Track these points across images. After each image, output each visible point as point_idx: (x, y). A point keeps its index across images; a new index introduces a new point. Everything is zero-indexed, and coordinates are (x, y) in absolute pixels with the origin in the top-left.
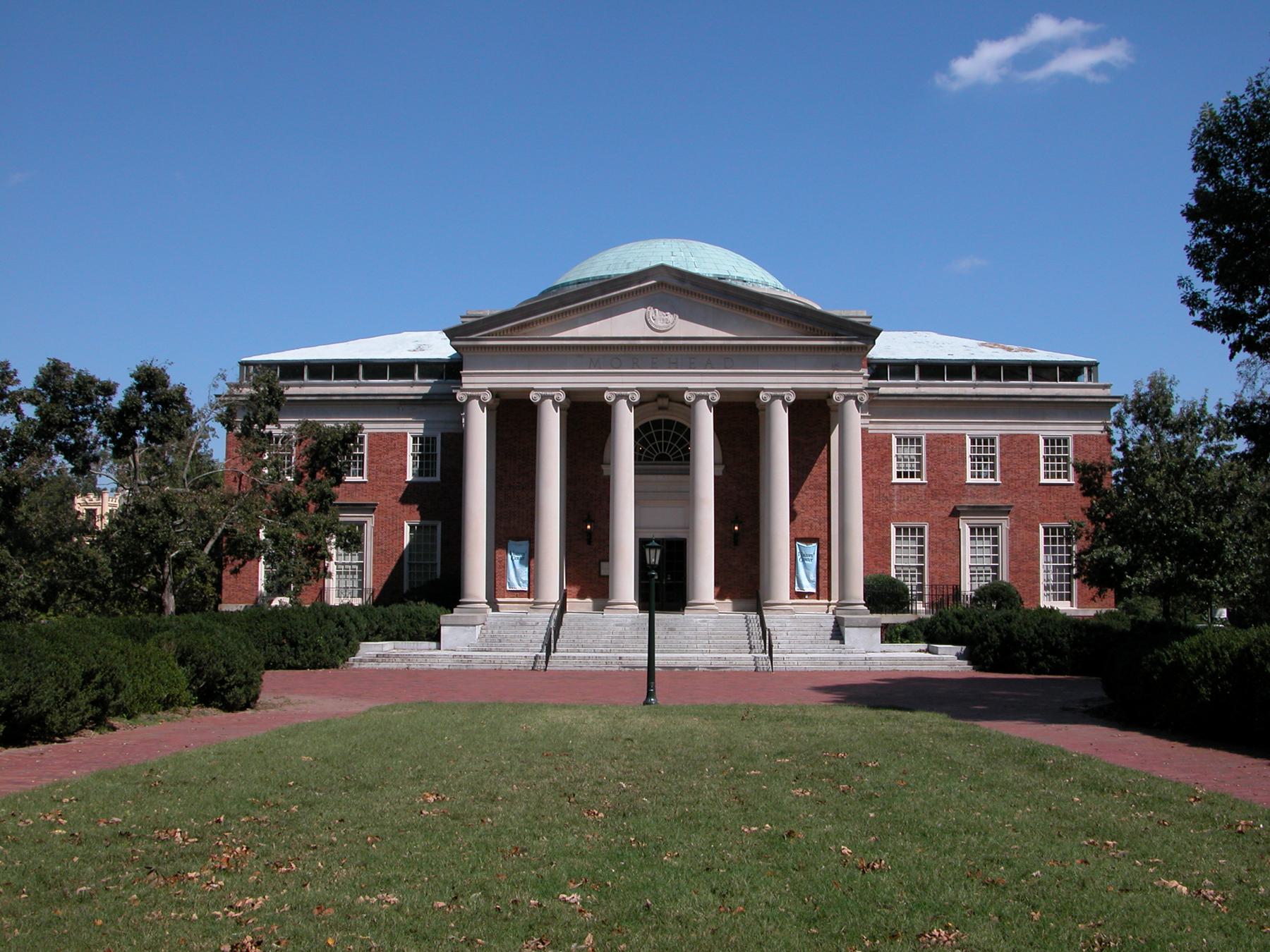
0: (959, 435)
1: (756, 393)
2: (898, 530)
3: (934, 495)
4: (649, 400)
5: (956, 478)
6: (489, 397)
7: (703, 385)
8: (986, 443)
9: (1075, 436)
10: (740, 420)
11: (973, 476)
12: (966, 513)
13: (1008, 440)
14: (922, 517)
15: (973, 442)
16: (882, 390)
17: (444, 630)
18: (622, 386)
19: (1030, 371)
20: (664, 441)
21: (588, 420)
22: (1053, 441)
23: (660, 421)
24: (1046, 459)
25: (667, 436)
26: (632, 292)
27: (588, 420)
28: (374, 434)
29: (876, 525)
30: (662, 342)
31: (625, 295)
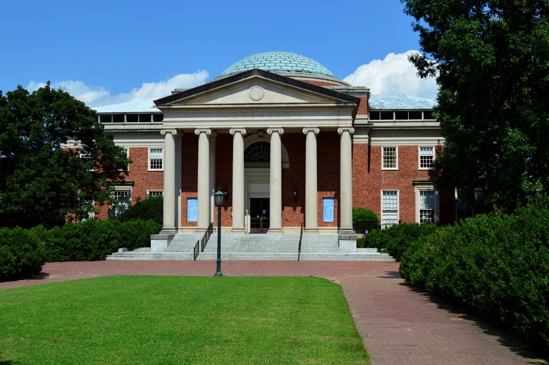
0: (415, 146)
1: (302, 128)
3: (402, 176)
4: (249, 134)
5: (413, 167)
6: (175, 132)
7: (275, 125)
8: (391, 150)
9: (130, 148)
10: (293, 140)
12: (418, 184)
13: (403, 149)
14: (397, 186)
15: (385, 149)
18: (238, 125)
19: (152, 116)
20: (258, 152)
21: (222, 141)
22: (388, 149)
23: (260, 142)
24: (385, 158)
25: (259, 149)
26: (242, 82)
27: (222, 141)
28: (132, 148)
29: (373, 190)
30: (256, 106)
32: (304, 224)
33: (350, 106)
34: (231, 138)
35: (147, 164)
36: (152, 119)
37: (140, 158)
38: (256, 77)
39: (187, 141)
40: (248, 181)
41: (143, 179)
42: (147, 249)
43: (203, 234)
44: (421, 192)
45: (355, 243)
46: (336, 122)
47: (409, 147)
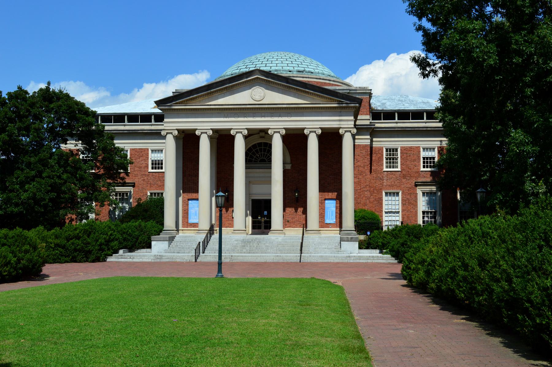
0: (417, 147)
2: (386, 193)
3: (404, 177)
4: (251, 134)
5: (416, 168)
7: (277, 126)
8: (393, 151)
9: (130, 149)
10: (295, 141)
11: (152, 168)
13: (405, 150)
14: (399, 187)
15: (387, 150)
16: (377, 125)
17: (153, 243)
18: (239, 126)
19: (153, 117)
20: (259, 153)
21: (223, 142)
22: (390, 150)
23: (261, 143)
24: (387, 159)
25: (261, 150)
26: (243, 82)
27: (223, 142)
29: (375, 191)
30: (257, 106)
31: (238, 84)
32: (305, 226)
33: (352, 107)
34: (232, 139)
35: (148, 165)
36: (153, 120)
37: (141, 159)
38: (258, 78)
39: (188, 142)
40: (249, 182)
41: (144, 180)
42: (148, 250)
43: (204, 235)
44: (424, 194)
45: (356, 244)
46: (338, 123)
47: (411, 148)
